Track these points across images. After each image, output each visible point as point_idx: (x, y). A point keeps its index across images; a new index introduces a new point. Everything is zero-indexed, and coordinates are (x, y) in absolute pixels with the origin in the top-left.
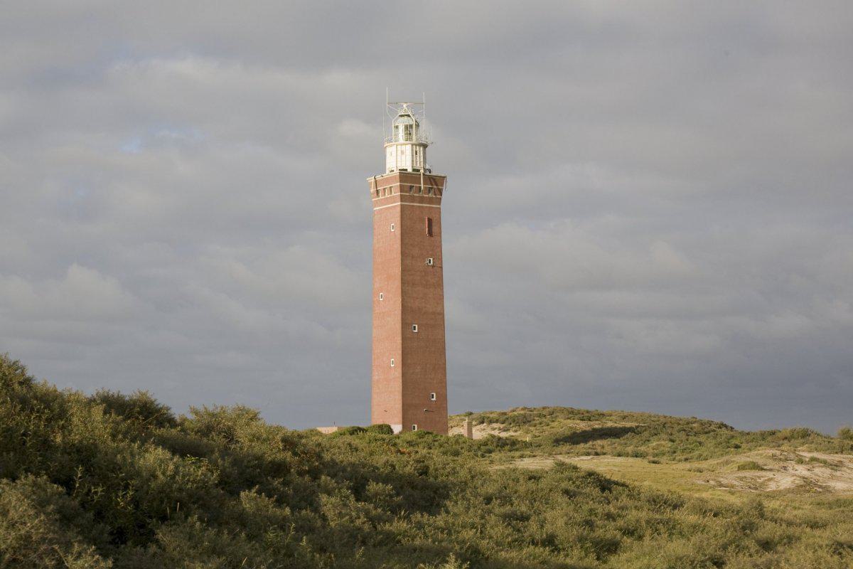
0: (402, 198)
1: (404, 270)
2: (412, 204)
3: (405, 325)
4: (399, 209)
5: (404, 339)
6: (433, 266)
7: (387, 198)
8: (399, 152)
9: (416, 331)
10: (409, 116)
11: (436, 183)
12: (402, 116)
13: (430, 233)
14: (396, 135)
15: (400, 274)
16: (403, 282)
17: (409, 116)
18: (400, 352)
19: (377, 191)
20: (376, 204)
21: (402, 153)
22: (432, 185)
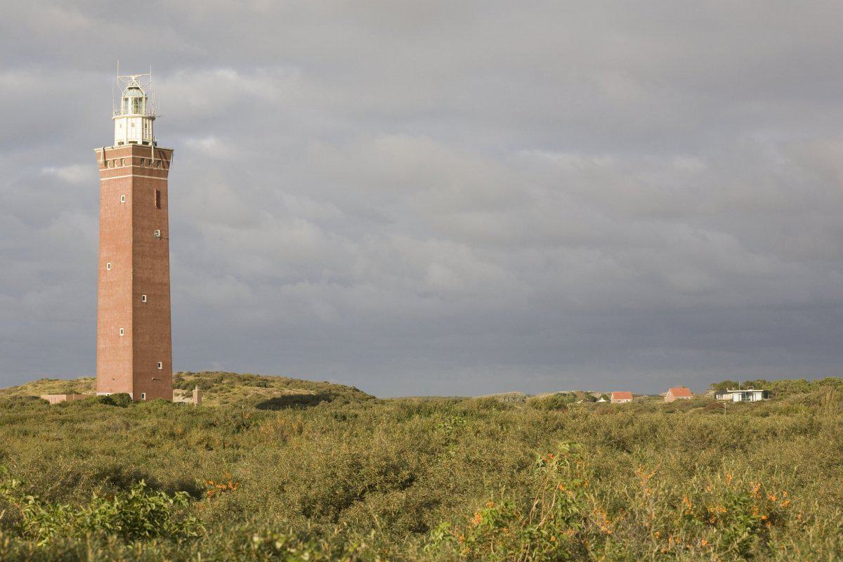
0: (134, 171)
1: (135, 242)
2: (142, 176)
3: (136, 295)
4: (130, 181)
5: (135, 309)
6: (161, 238)
7: (110, 170)
8: (130, 125)
9: (145, 301)
10: (138, 88)
11: (165, 156)
12: (130, 88)
13: (158, 205)
14: (126, 108)
15: (131, 244)
16: (135, 254)
17: (138, 88)
18: (131, 322)
19: (106, 163)
20: (104, 174)
21: (133, 125)
22: (161, 158)
